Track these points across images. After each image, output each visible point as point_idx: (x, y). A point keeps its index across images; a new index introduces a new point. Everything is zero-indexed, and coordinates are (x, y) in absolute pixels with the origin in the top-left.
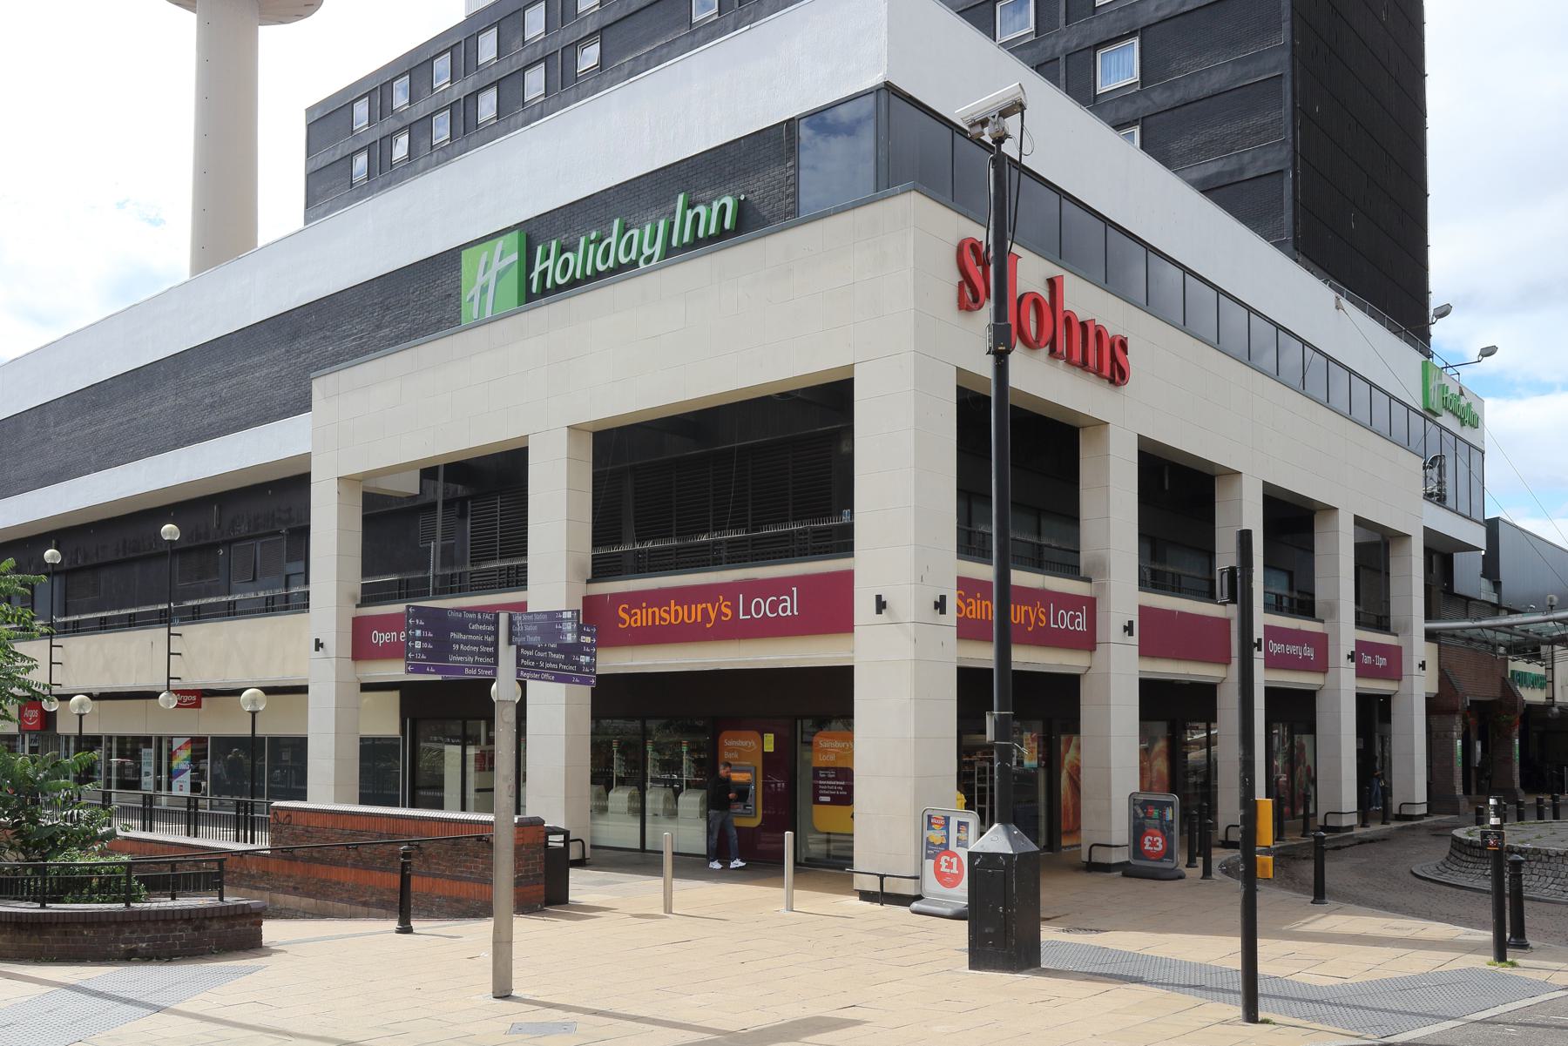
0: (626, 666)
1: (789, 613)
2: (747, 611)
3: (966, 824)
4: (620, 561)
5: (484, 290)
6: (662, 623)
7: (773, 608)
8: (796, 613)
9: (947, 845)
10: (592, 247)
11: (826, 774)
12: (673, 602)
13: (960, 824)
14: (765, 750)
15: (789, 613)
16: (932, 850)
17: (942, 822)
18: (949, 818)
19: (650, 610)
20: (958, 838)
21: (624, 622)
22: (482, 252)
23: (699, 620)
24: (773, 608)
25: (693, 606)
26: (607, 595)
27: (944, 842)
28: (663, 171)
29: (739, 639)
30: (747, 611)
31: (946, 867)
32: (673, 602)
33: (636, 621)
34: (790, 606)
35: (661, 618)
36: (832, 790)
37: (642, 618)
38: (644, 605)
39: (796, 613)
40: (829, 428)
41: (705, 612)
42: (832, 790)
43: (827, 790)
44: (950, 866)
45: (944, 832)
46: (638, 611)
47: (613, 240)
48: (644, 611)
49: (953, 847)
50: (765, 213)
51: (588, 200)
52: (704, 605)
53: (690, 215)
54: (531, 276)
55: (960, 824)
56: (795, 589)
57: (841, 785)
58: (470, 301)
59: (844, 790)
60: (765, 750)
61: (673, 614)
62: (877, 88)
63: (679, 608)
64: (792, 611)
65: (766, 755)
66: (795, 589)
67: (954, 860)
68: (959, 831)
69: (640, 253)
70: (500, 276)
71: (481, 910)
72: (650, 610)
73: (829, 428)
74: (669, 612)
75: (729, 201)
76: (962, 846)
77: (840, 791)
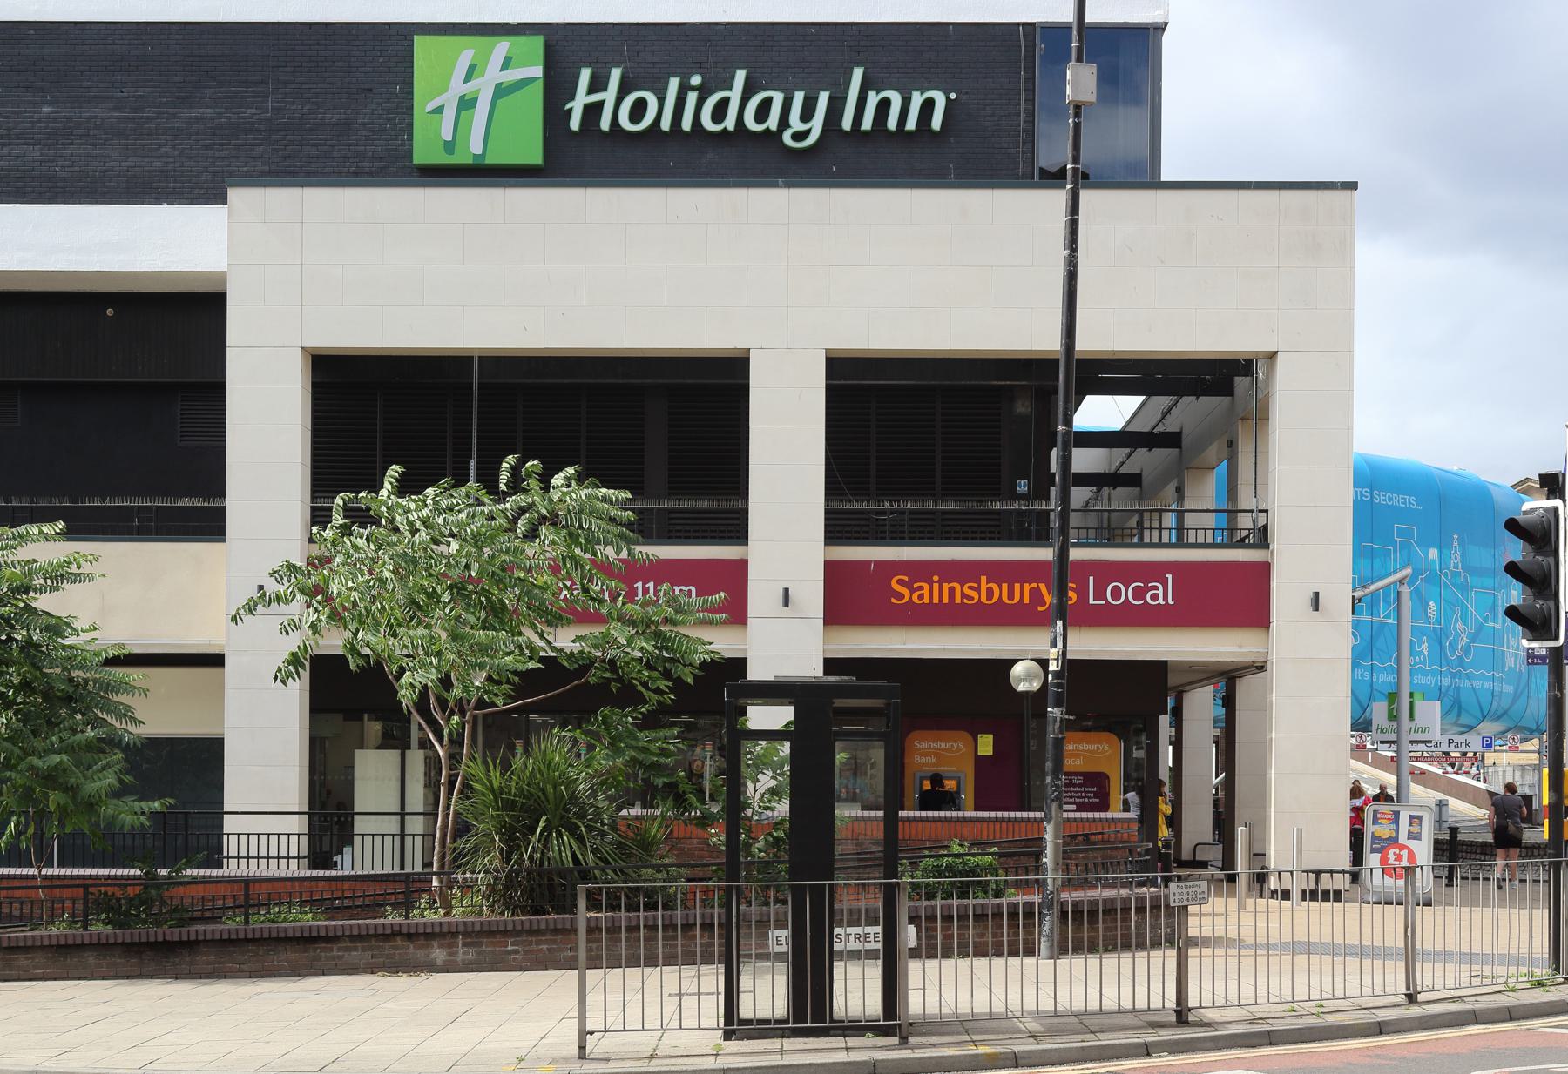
0: (891, 650)
1: (1161, 601)
2: (1100, 594)
3: (1420, 818)
4: (738, 519)
5: (466, 104)
6: (966, 601)
7: (1139, 593)
8: (1170, 602)
9: (1396, 839)
10: (692, 97)
11: (1070, 780)
12: (983, 579)
13: (1411, 817)
14: (979, 754)
15: (1161, 601)
16: (1379, 844)
17: (1392, 817)
18: (1399, 812)
19: (946, 586)
20: (1409, 831)
21: (901, 596)
22: (466, 50)
23: (1026, 600)
24: (1139, 593)
25: (1017, 586)
26: (871, 561)
27: (1394, 835)
28: (818, 27)
29: (1080, 626)
30: (1100, 594)
31: (1395, 860)
32: (983, 579)
33: (921, 597)
34: (1162, 594)
35: (964, 595)
36: (1078, 797)
37: (930, 593)
38: (936, 578)
39: (1170, 602)
40: (1008, 383)
41: (1035, 593)
42: (1078, 797)
43: (1071, 797)
44: (1399, 858)
45: (1393, 826)
46: (926, 586)
47: (735, 95)
48: (936, 586)
49: (1403, 839)
50: (987, 124)
51: (675, 27)
52: (1034, 585)
53: (873, 99)
54: (568, 106)
55: (1411, 817)
56: (1169, 577)
57: (1091, 792)
58: (432, 112)
59: (1095, 797)
60: (979, 754)
61: (981, 592)
62: (1155, 26)
63: (994, 586)
64: (1165, 598)
65: (980, 761)
66: (1169, 577)
67: (1405, 853)
68: (1410, 825)
69: (784, 122)
70: (501, 91)
71: (571, 966)
72: (946, 586)
73: (1008, 383)
74: (978, 590)
75: (940, 99)
76: (1414, 838)
77: (1089, 798)
